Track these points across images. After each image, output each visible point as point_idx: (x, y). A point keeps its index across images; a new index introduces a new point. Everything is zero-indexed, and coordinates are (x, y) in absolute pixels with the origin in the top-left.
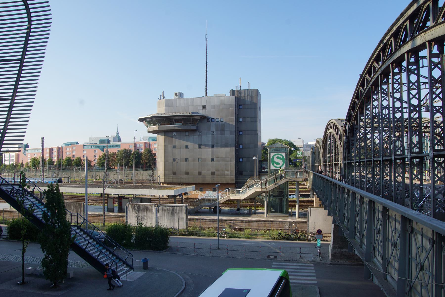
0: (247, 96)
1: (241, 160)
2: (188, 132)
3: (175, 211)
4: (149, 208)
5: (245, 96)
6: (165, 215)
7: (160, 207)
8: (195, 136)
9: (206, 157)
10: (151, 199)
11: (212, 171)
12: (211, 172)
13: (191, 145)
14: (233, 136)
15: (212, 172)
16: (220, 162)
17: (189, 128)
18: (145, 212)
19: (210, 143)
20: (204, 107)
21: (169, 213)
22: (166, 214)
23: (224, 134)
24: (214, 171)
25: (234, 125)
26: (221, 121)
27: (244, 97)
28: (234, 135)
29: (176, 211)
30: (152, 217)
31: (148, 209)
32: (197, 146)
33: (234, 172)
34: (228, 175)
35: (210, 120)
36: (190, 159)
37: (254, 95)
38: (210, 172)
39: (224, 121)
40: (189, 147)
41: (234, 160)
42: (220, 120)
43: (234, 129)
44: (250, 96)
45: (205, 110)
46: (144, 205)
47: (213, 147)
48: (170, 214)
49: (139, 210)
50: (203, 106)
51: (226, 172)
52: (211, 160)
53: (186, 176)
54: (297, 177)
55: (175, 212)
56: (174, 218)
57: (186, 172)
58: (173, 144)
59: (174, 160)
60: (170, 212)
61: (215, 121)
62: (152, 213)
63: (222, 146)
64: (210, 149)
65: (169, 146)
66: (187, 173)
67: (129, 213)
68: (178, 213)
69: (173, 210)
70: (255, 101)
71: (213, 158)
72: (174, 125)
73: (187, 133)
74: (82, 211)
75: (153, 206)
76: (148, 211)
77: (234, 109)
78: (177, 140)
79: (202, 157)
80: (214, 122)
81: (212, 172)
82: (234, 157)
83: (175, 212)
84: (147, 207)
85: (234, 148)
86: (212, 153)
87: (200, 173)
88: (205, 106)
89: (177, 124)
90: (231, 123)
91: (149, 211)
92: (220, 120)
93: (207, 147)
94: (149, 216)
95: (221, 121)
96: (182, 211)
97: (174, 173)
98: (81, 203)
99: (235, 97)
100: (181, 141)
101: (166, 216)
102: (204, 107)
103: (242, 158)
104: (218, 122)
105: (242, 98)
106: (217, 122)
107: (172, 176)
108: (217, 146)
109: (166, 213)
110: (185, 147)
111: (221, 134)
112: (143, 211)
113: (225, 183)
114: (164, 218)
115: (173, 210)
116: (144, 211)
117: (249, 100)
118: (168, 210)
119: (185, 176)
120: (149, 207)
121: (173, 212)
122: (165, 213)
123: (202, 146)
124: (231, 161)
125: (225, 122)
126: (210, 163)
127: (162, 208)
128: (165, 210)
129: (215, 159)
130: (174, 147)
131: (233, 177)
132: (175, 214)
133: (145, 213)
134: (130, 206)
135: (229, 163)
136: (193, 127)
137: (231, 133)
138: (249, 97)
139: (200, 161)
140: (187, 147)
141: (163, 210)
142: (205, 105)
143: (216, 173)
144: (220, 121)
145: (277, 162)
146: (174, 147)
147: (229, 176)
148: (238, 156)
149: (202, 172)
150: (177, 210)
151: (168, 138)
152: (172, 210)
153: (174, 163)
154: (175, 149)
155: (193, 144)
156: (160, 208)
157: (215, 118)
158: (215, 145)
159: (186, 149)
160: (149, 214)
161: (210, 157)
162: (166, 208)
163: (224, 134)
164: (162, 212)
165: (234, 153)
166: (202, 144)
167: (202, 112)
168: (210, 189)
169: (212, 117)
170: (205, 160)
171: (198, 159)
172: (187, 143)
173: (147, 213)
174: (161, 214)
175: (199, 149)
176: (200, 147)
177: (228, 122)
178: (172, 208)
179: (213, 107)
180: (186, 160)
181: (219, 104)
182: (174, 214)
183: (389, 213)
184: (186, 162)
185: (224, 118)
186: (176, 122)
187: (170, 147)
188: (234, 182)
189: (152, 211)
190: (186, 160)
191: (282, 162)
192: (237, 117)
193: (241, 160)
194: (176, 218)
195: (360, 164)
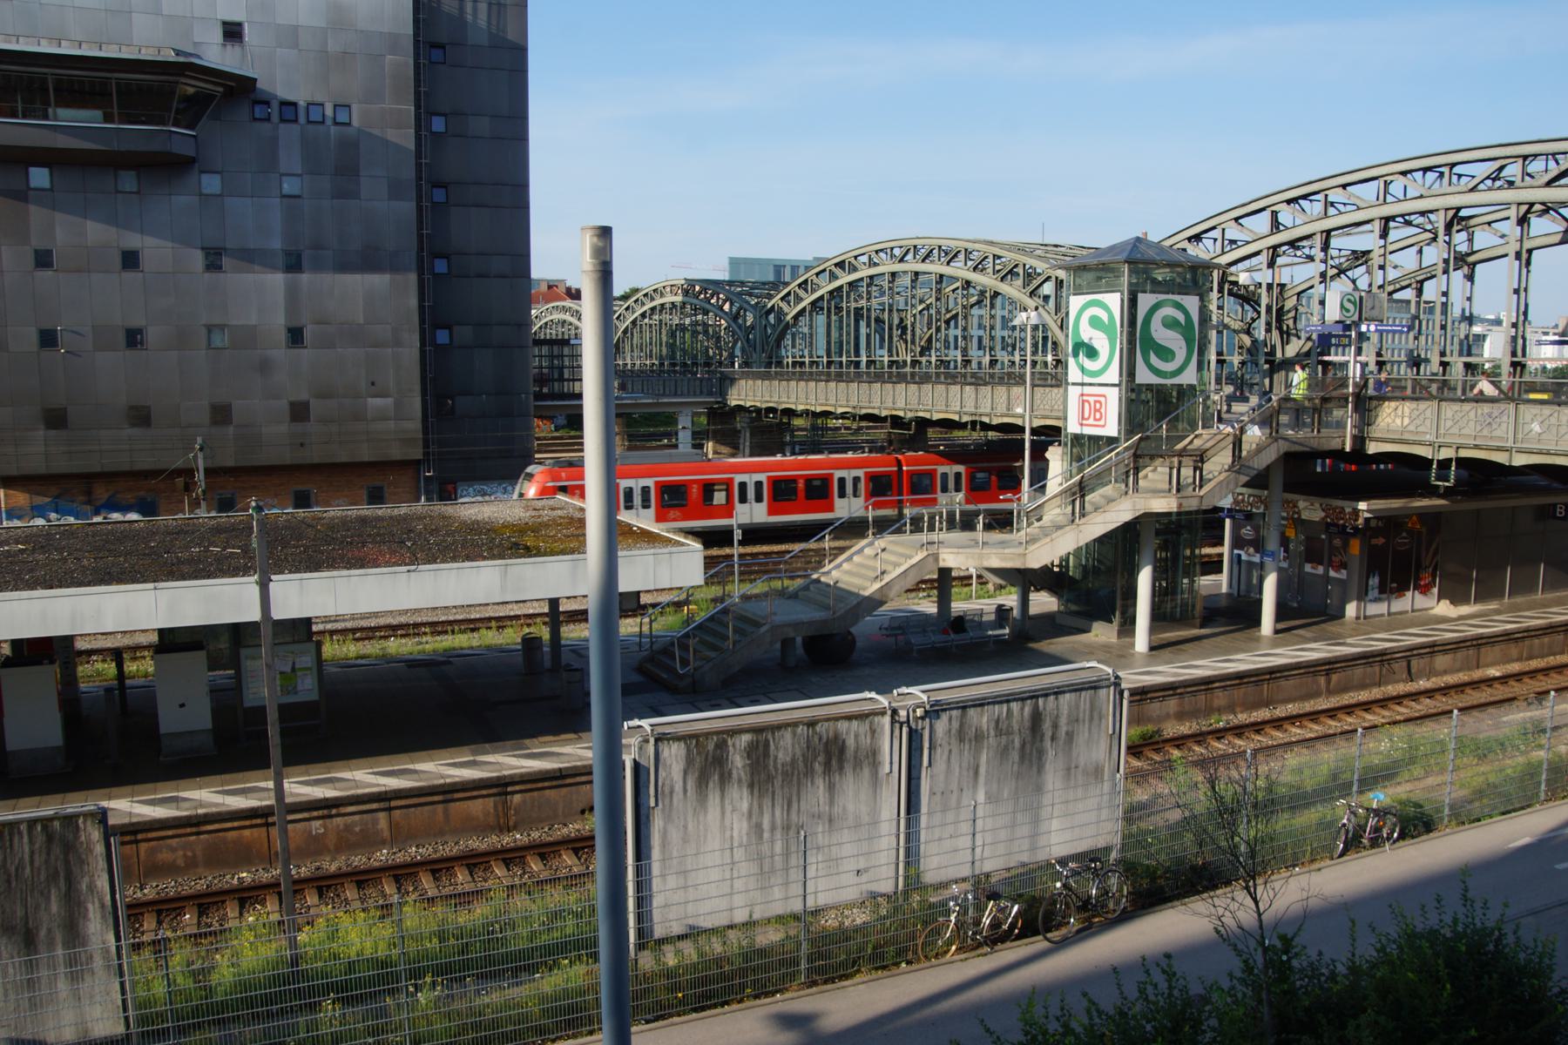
1: (442, 337)
2: (133, 173)
4: (851, 742)
6: (976, 773)
8: (180, 201)
9: (253, 322)
10: (315, 628)
11: (292, 399)
12: (286, 401)
13: (153, 249)
14: (408, 207)
15: (293, 405)
17: (155, 146)
18: (820, 783)
19: (277, 244)
20: (232, 32)
21: (1004, 752)
22: (982, 770)
24: (303, 396)
25: (412, 147)
28: (413, 204)
29: (1055, 726)
31: (842, 749)
34: (385, 419)
35: (274, 110)
36: (153, 335)
39: (355, 123)
40: (147, 260)
42: (329, 112)
43: (409, 173)
45: (237, 48)
46: (811, 724)
47: (293, 264)
50: (225, 23)
51: (375, 402)
52: (282, 336)
53: (136, 431)
54: (1319, 431)
55: (1048, 734)
57: (132, 408)
58: (37, 242)
59: (48, 339)
61: (302, 119)
63: (344, 266)
64: (277, 280)
66: (141, 417)
67: (668, 818)
68: (1070, 736)
69: (1037, 717)
70: (511, 35)
71: (295, 324)
72: (46, 117)
73: (128, 181)
74: (93, 911)
75: (887, 720)
76: (841, 768)
77: (411, 61)
80: (296, 121)
81: (293, 405)
83: (1048, 734)
84: (837, 736)
85: (413, 277)
86: (292, 295)
87: (221, 414)
88: (240, 25)
89: (68, 117)
90: (392, 135)
91: (848, 768)
92: (329, 112)
93: (256, 268)
94: (851, 807)
95: (309, 122)
97: (56, 419)
100: (89, 223)
101: (982, 779)
102: (232, 32)
103: (449, 327)
104: (321, 127)
106: (310, 127)
107: (41, 433)
108: (318, 267)
109: (984, 758)
111: (341, 194)
112: (797, 774)
113: (372, 459)
114: (967, 800)
115: (1037, 717)
116: (809, 772)
118: (999, 732)
120: (852, 733)
121: (1033, 743)
122: (976, 757)
124: (398, 343)
125: (359, 130)
126: (280, 353)
127: (956, 725)
128: (979, 737)
130: (43, 260)
131: (414, 425)
134: (674, 754)
137: (395, 191)
140: (130, 260)
141: (961, 740)
143: (316, 407)
144: (329, 122)
145: (1160, 342)
146: (43, 260)
147: (391, 425)
148: (433, 317)
150: (1063, 721)
152: (1027, 724)
154: (47, 274)
155: (170, 244)
156: (941, 725)
157: (302, 103)
158: (307, 256)
159: (129, 276)
160: (852, 793)
162: (981, 719)
164: (955, 751)
165: (413, 302)
167: (217, 55)
168: (276, 495)
169: (283, 93)
170: (246, 338)
171: (204, 331)
173: (831, 788)
175: (207, 275)
176: (213, 265)
177: (376, 132)
178: (1027, 710)
179: (292, 35)
180: (134, 338)
181: (324, 25)
183: (854, 529)
185: (355, 108)
188: (417, 453)
190: (134, 338)
192: (425, 108)
193: (442, 337)
194: (1049, 786)
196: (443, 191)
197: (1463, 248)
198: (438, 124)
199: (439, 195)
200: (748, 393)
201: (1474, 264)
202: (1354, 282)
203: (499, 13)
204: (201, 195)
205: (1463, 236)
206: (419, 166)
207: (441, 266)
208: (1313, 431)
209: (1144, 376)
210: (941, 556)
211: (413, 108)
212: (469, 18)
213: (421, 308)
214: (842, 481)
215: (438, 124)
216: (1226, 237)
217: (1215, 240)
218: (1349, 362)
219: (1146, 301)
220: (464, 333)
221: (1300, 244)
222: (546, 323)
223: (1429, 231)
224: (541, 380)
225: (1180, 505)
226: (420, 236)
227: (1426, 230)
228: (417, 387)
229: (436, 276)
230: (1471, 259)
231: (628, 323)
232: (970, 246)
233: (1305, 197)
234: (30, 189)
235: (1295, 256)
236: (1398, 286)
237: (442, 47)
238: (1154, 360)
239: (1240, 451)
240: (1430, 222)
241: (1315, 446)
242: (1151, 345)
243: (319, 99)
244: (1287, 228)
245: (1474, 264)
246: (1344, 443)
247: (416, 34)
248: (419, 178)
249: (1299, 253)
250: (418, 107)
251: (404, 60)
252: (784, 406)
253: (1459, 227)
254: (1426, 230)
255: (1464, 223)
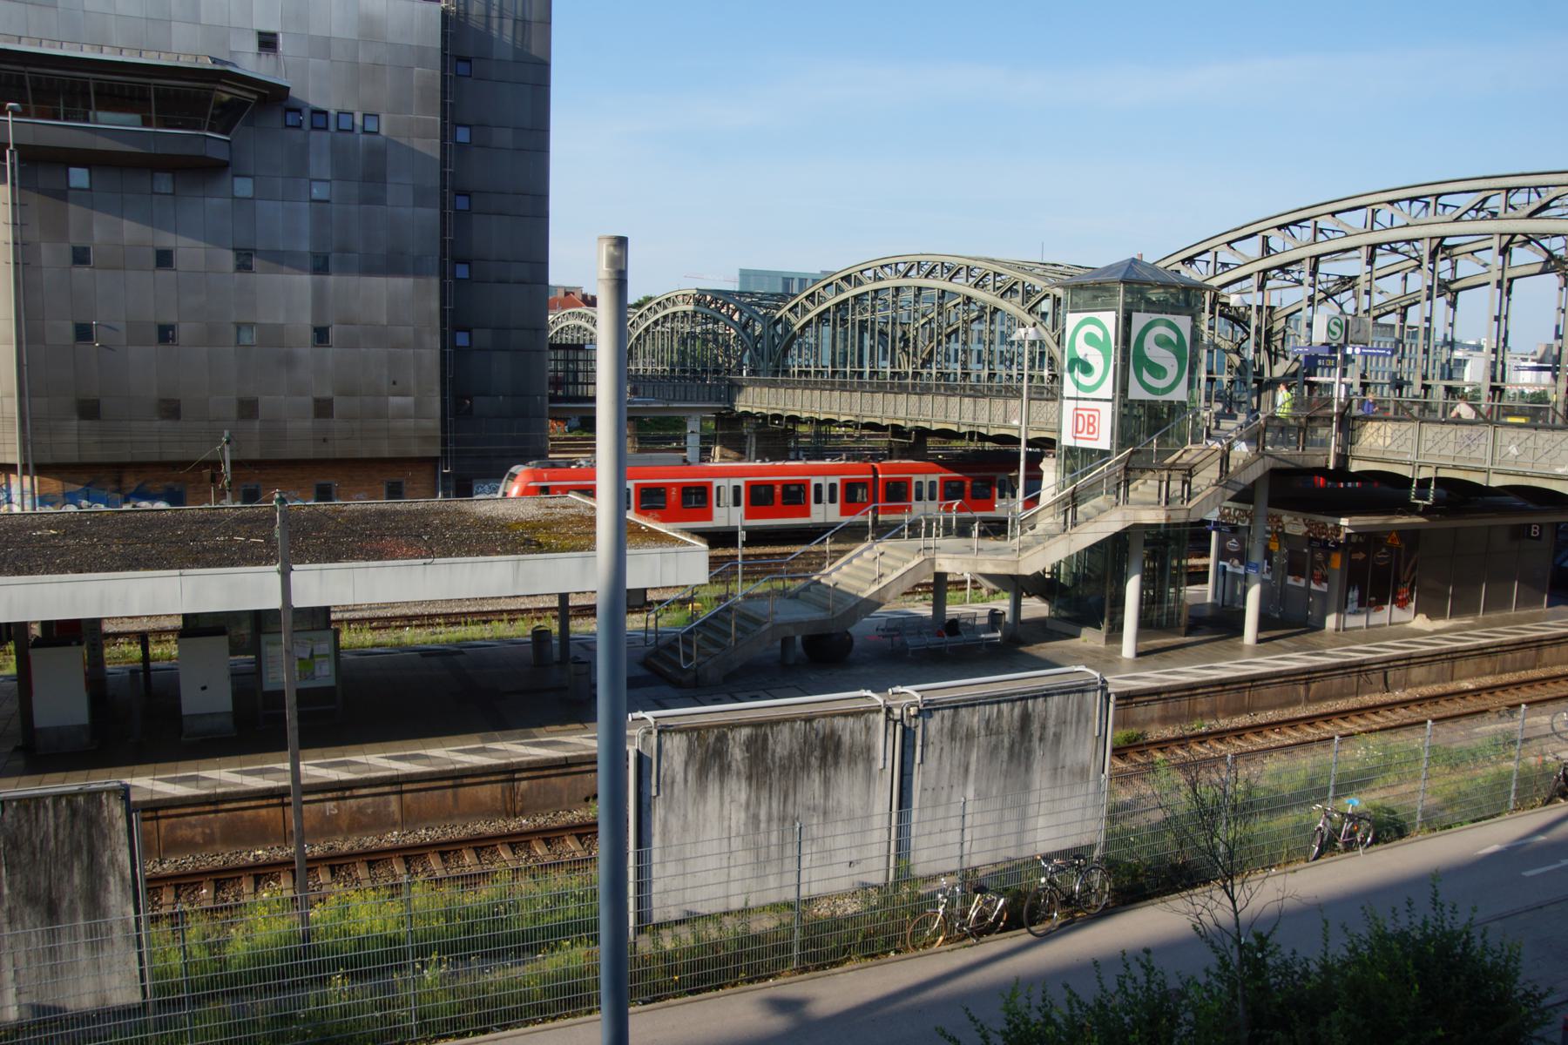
0: (501, 17)
1: (462, 339)
2: (168, 176)
3: (1035, 727)
4: (846, 738)
5: (488, 16)
6: (967, 770)
7: (937, 716)
8: (211, 204)
9: (281, 321)
10: (333, 617)
13: (187, 249)
14: (433, 213)
16: (363, 350)
17: (188, 150)
18: (816, 777)
19: (305, 246)
20: (267, 42)
21: (993, 751)
22: (973, 768)
23: (381, 201)
24: (328, 394)
25: (437, 155)
26: (365, 132)
27: (483, 20)
28: (438, 211)
29: (1043, 727)
30: (868, 805)
31: (838, 744)
32: (228, 259)
33: (438, 398)
35: (306, 118)
36: (184, 331)
37: (534, 17)
38: (308, 401)
39: (383, 132)
40: (180, 260)
41: (437, 340)
43: (434, 181)
44: (515, 21)
48: (1004, 755)
49: (760, 766)
50: (260, 34)
51: (395, 401)
52: (308, 335)
55: (1037, 735)
56: (1027, 788)
57: (163, 401)
58: (75, 240)
59: (84, 333)
60: (1006, 743)
61: (332, 127)
62: (869, 776)
63: (370, 269)
65: (43, 245)
66: (171, 410)
67: (669, 808)
68: (1057, 737)
69: (1026, 718)
70: (535, 51)
71: (321, 324)
72: (87, 120)
73: (164, 183)
74: (114, 884)
75: (882, 717)
76: (836, 763)
77: (438, 73)
78: (98, 217)
79: (263, 321)
80: (326, 128)
82: (438, 324)
83: (1037, 735)
84: (833, 732)
86: (319, 297)
87: (248, 409)
88: (275, 35)
89: (108, 120)
90: (418, 144)
92: (358, 120)
94: (845, 801)
95: (339, 130)
96: (1078, 721)
97: (89, 410)
98: (94, 795)
99: (445, 14)
100: (126, 223)
101: (972, 777)
102: (267, 42)
103: (469, 331)
104: (350, 135)
105: (472, 23)
106: (340, 136)
109: (974, 757)
110: (152, 261)
111: (367, 200)
112: (794, 768)
115: (1026, 718)
116: (806, 766)
117: (508, 36)
118: (989, 731)
119: (158, 424)
120: (847, 729)
121: (1022, 743)
123: (256, 262)
124: (419, 344)
125: (387, 139)
126: (306, 351)
127: (947, 723)
128: (970, 736)
129: (333, 333)
130: (81, 257)
131: (433, 424)
132: (1038, 753)
133: (812, 786)
134: (676, 746)
135: (411, 351)
136: (212, 142)
137: (420, 199)
138: (508, 23)
139: (248, 342)
140: (164, 259)
141: (953, 739)
142: (271, 28)
143: (339, 404)
144: (358, 130)
148: (453, 320)
149: (264, 400)
150: (1051, 723)
151: (35, 199)
152: (1017, 724)
153: (82, 347)
155: (202, 244)
156: (934, 724)
157: (333, 112)
159: (162, 274)
160: (847, 788)
161: (305, 321)
162: (973, 719)
163: (381, 201)
165: (435, 305)
166: (260, 246)
167: (251, 64)
169: (315, 101)
170: (274, 336)
171: (233, 330)
172: (167, 240)
173: (826, 782)
174: (940, 768)
175: (237, 275)
176: (244, 266)
177: (403, 141)
178: (1017, 711)
179: (324, 46)
180: (166, 334)
182: (1029, 752)
184: (161, 348)
185: (383, 117)
186: (104, 106)
187: (51, 255)
188: (435, 451)
189: (869, 760)
190: (166, 334)
191: (1175, 362)
192: (450, 117)
193: (462, 339)
195: (572, 361)
196: (465, 199)
197: (1447, 276)
198: (463, 135)
199: (462, 203)
200: (755, 400)
201: (1457, 291)
202: (1340, 306)
203: (524, 27)
204: (234, 197)
205: (1447, 263)
206: (443, 175)
207: (462, 271)
208: (1298, 449)
209: (1136, 392)
210: (937, 562)
211: (439, 119)
212: (495, 33)
213: (443, 312)
214: (818, 487)
215: (463, 135)
216: (1218, 260)
217: (1208, 262)
218: (1334, 383)
219: (1140, 320)
220: (483, 337)
221: (1289, 268)
222: (562, 329)
223: (1415, 259)
224: (557, 383)
225: (1168, 518)
226: (443, 242)
227: (1411, 258)
228: (437, 388)
229: (457, 280)
230: (1454, 286)
231: (641, 330)
232: (972, 263)
233: (1295, 223)
234: (69, 188)
235: (1285, 279)
236: (1383, 311)
237: (468, 60)
238: (1146, 376)
239: (1228, 466)
240: (1416, 250)
241: (1300, 462)
242: (1144, 363)
243: (349, 108)
244: (1277, 253)
245: (1457, 291)
246: (1327, 461)
247: (444, 48)
248: (443, 186)
249: (1288, 277)
250: (444, 118)
251: (432, 72)
252: (789, 413)
253: (1443, 256)
254: (1411, 258)
255: (1448, 252)
